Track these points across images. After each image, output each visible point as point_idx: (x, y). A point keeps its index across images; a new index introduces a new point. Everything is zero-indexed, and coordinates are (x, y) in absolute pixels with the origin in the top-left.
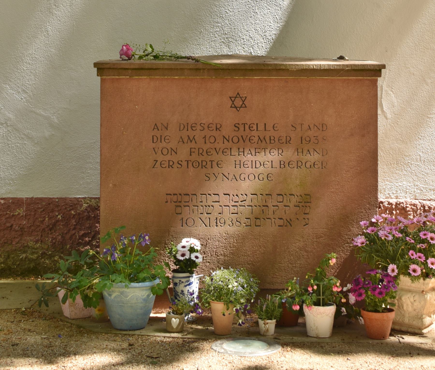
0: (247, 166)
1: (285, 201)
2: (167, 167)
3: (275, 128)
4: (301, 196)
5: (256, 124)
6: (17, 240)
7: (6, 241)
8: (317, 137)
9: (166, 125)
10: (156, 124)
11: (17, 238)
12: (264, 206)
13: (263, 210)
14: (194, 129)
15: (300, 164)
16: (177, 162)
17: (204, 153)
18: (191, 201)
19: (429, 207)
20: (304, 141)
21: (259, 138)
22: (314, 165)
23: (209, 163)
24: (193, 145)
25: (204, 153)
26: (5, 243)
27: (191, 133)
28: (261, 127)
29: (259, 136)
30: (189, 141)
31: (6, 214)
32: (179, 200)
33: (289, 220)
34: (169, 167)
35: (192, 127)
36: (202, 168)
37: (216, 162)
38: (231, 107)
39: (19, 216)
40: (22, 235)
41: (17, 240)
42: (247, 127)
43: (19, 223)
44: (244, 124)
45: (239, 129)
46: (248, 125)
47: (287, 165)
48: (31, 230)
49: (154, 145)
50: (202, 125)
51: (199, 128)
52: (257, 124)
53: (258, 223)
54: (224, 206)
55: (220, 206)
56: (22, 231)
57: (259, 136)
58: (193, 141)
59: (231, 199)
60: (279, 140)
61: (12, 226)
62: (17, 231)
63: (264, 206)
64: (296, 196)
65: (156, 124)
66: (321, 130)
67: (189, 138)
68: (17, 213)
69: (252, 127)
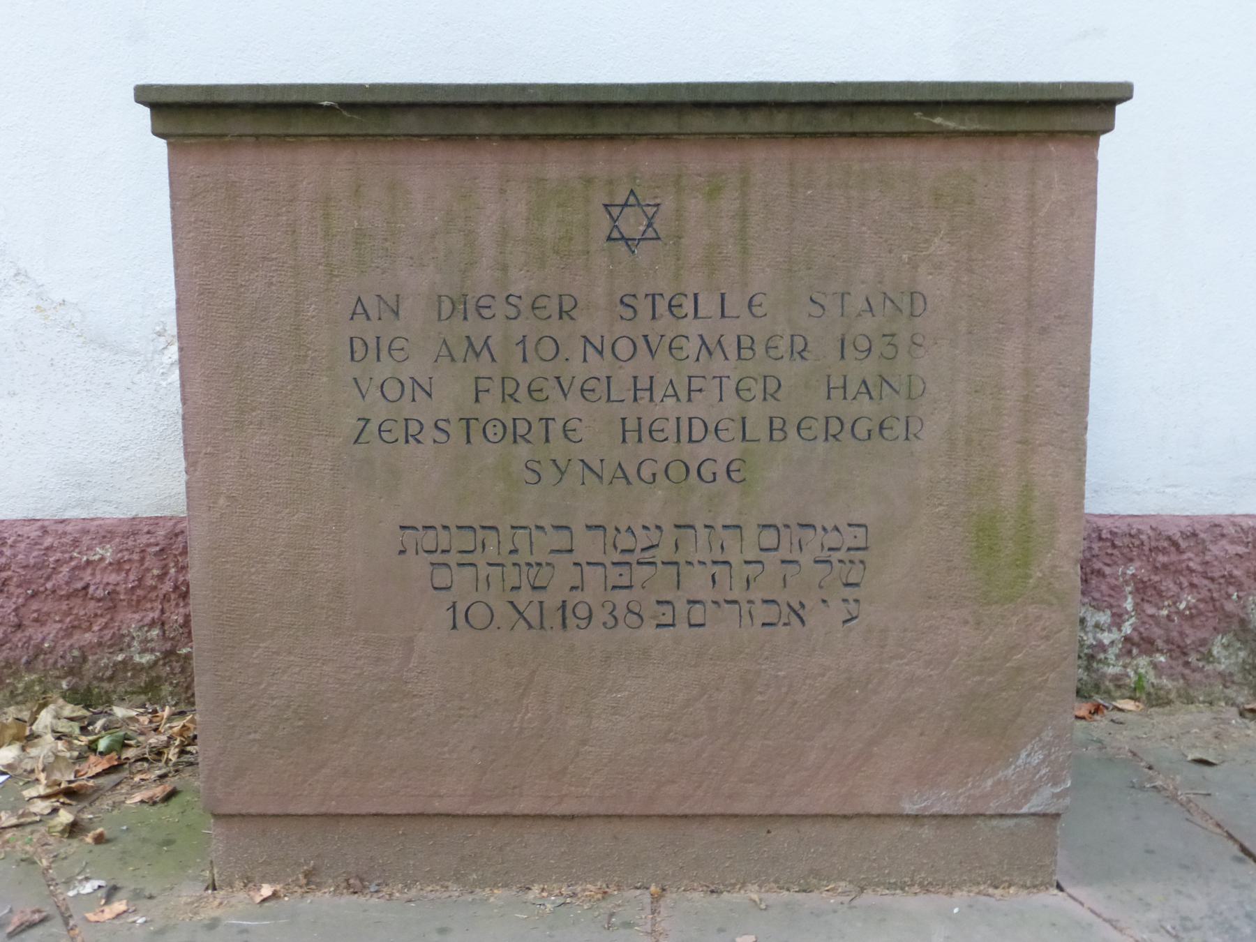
0: (661, 436)
1: (785, 543)
2: (402, 440)
3: (754, 309)
4: (837, 530)
5: (691, 297)
6: (102, 621)
7: (76, 623)
8: (893, 335)
9: (392, 304)
10: (359, 299)
11: (102, 616)
12: (715, 562)
13: (713, 576)
14: (486, 313)
15: (834, 427)
16: (432, 424)
17: (522, 394)
18: (480, 549)
19: (1111, 532)
20: (849, 351)
21: (704, 343)
22: (881, 428)
23: (538, 428)
24: (484, 367)
25: (522, 394)
26: (74, 627)
27: (475, 327)
28: (709, 306)
29: (701, 336)
30: (470, 353)
31: (71, 558)
32: (445, 546)
33: (797, 607)
34: (407, 441)
35: (478, 308)
36: (515, 441)
37: (560, 423)
38: (609, 239)
39: (103, 565)
40: (113, 608)
41: (102, 621)
42: (662, 306)
43: (105, 581)
44: (653, 296)
45: (635, 311)
46: (668, 298)
47: (792, 432)
48: (134, 598)
49: (356, 370)
50: (513, 300)
51: (500, 309)
52: (696, 296)
53: (697, 617)
54: (589, 563)
55: (575, 564)
56: (111, 600)
57: (701, 336)
58: (485, 353)
59: (610, 541)
60: (767, 349)
61: (86, 587)
62: (99, 600)
63: (715, 562)
64: (819, 530)
65: (359, 299)
66: (907, 311)
67: (471, 344)
68: (97, 557)
69: (680, 306)
